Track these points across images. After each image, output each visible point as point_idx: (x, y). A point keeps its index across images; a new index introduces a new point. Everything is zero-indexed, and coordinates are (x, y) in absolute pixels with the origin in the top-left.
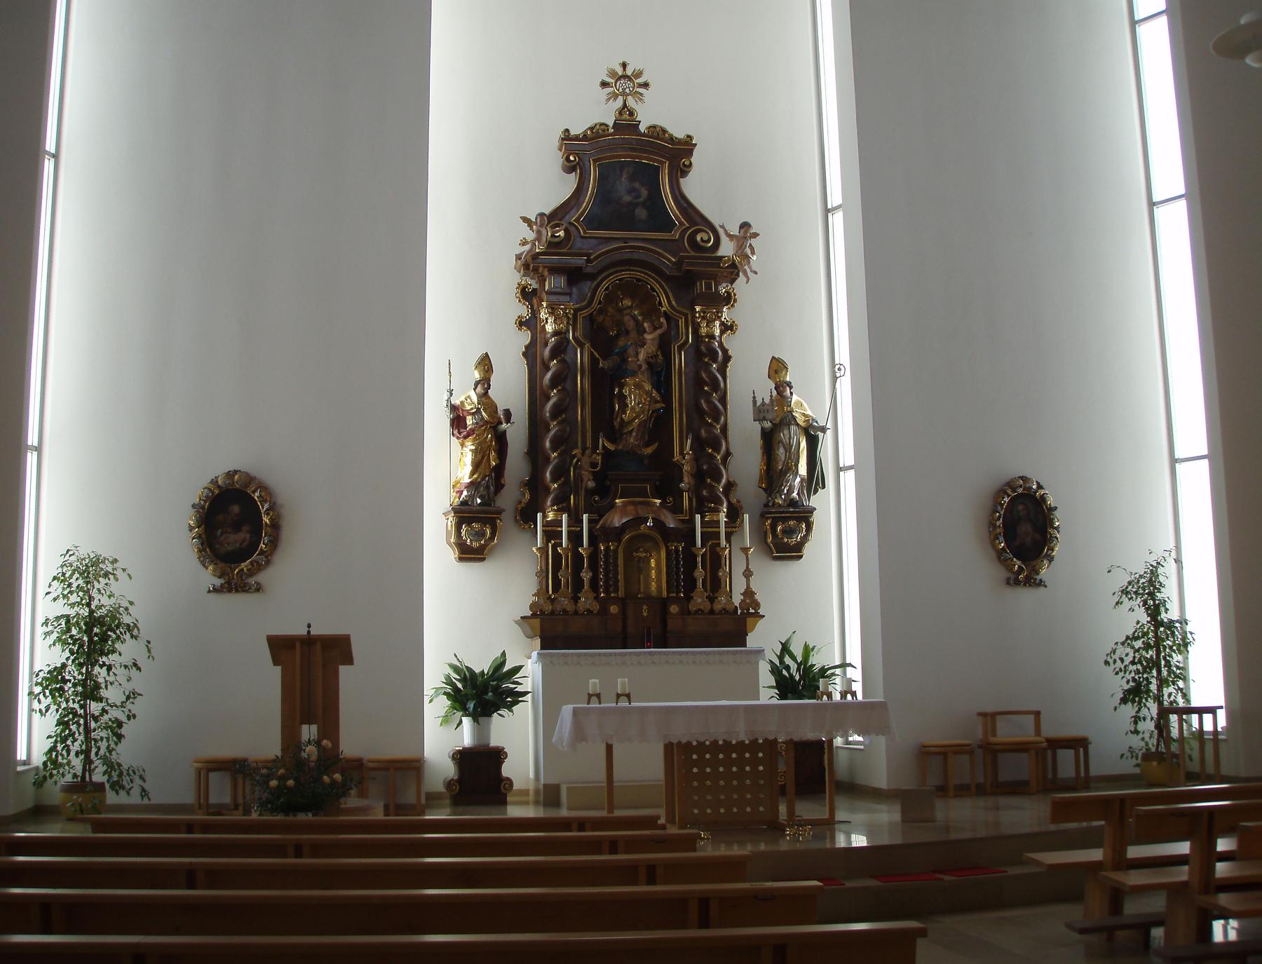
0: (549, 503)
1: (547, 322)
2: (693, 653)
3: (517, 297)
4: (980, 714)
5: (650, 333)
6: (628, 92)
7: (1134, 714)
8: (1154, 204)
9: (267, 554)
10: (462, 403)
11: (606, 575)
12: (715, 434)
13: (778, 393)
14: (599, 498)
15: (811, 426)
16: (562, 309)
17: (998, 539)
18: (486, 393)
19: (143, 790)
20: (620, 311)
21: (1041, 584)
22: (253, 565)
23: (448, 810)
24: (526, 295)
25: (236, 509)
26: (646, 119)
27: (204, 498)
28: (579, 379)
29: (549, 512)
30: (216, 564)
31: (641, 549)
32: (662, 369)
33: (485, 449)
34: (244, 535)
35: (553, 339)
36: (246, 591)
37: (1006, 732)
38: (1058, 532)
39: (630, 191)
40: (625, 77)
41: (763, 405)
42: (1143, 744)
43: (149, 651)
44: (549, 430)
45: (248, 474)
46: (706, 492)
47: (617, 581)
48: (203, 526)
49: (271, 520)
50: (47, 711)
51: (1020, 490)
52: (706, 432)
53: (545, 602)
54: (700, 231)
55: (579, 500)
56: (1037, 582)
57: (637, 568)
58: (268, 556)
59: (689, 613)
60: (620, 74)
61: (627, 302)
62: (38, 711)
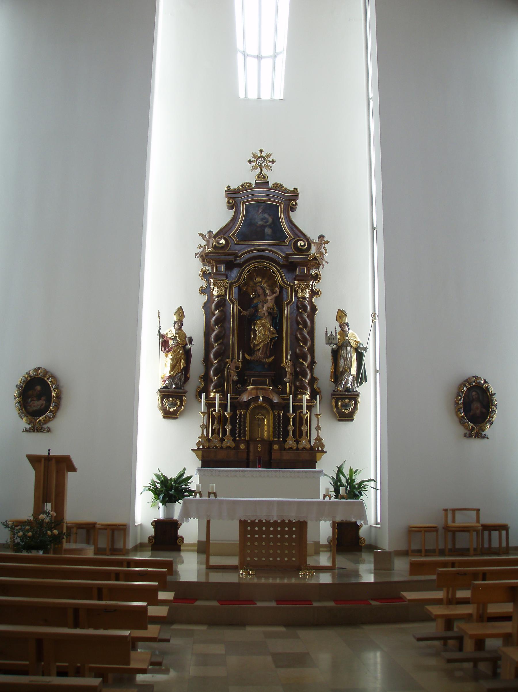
0: (211, 388)
1: (214, 290)
3: (200, 277)
5: (270, 296)
6: (263, 165)
9: (53, 412)
10: (167, 333)
11: (239, 428)
12: (304, 351)
13: (341, 329)
16: (221, 283)
20: (255, 283)
21: (485, 437)
23: (150, 553)
25: (38, 388)
28: (231, 320)
29: (211, 393)
30: (27, 417)
31: (260, 414)
32: (277, 316)
33: (178, 358)
34: (42, 402)
35: (217, 299)
36: (42, 432)
37: (461, 520)
40: (262, 157)
41: (331, 336)
44: (213, 348)
45: (45, 370)
46: (299, 383)
47: (245, 431)
48: (21, 397)
51: (474, 384)
52: (299, 350)
53: (205, 442)
55: (229, 387)
57: (257, 424)
58: (54, 413)
59: (285, 449)
61: (259, 279)
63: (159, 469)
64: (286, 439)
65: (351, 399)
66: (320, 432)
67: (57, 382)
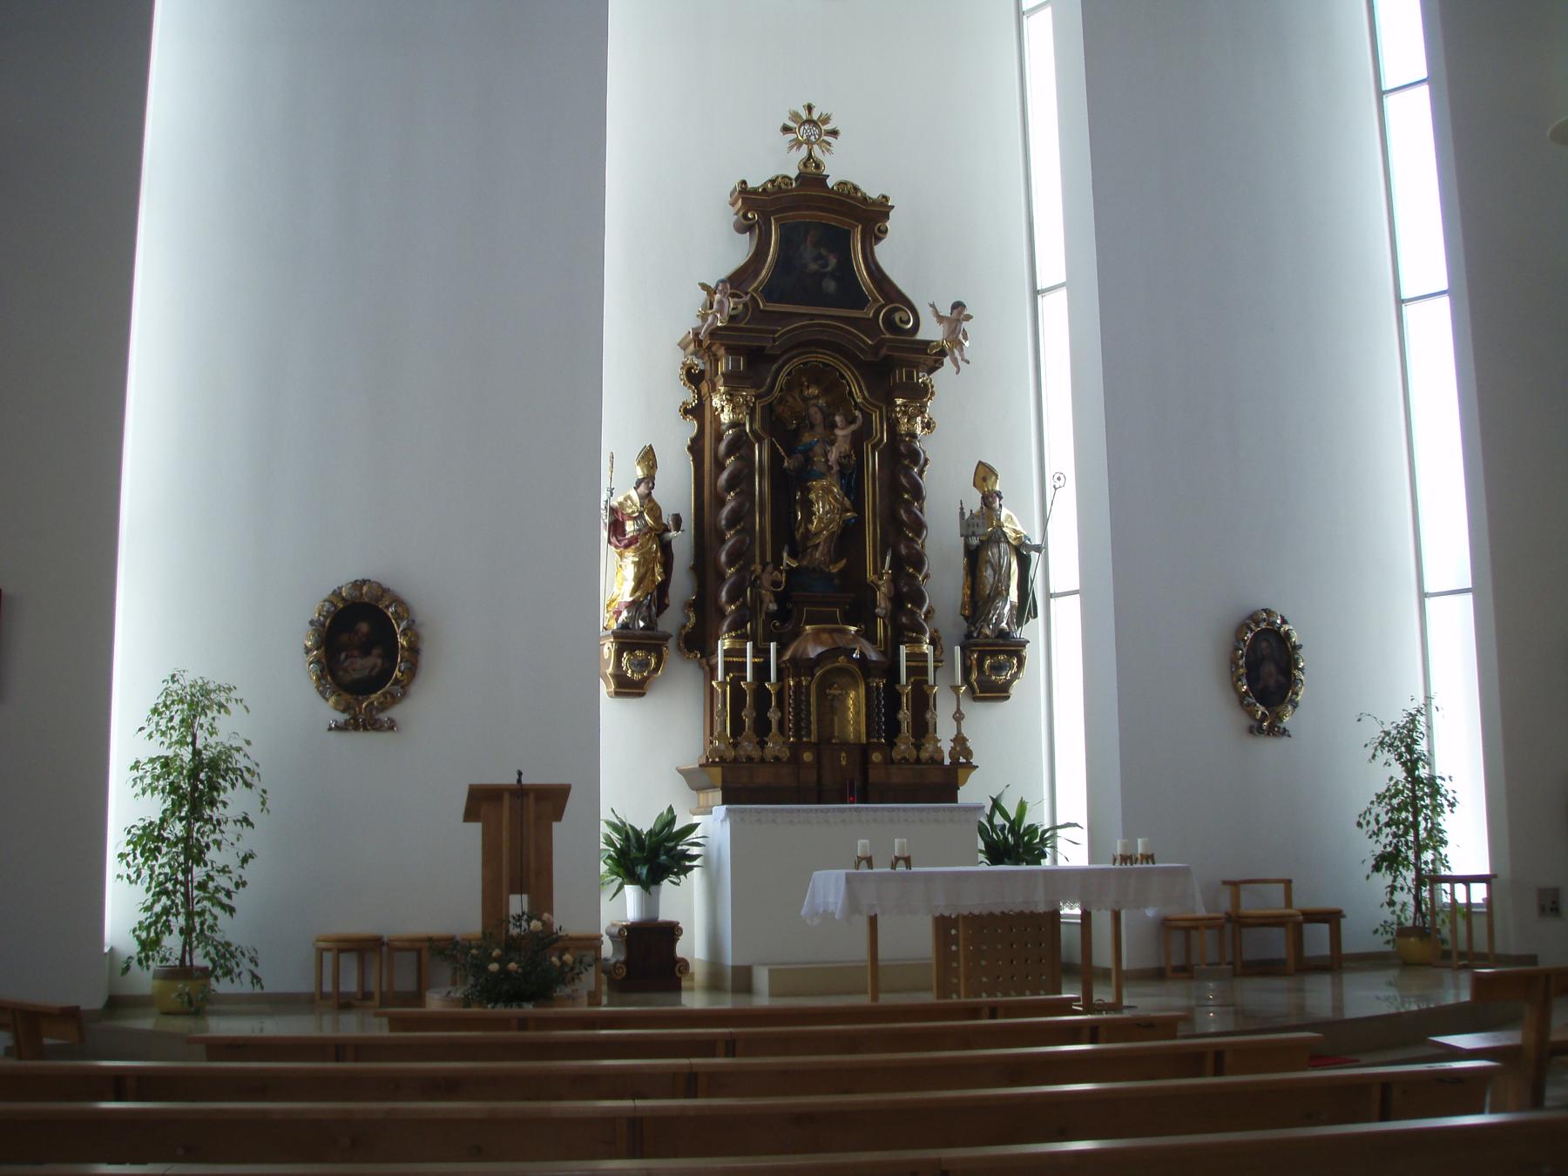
1: (723, 410)
2: (905, 810)
4: (1225, 883)
5: (842, 429)
6: (814, 140)
7: (1390, 883)
8: (1403, 301)
12: (916, 549)
14: (783, 626)
15: (1023, 544)
17: (1240, 680)
18: (649, 494)
19: (254, 976)
20: (805, 400)
21: (1284, 733)
22: (386, 697)
24: (693, 378)
25: (364, 627)
26: (837, 170)
27: (325, 613)
32: (853, 472)
34: (373, 661)
35: (730, 432)
37: (1252, 903)
38: (1303, 673)
39: (815, 260)
40: (810, 121)
41: (973, 519)
42: (1395, 917)
43: (263, 803)
45: (379, 585)
47: (810, 722)
49: (409, 642)
50: (138, 876)
51: (1263, 625)
54: (897, 309)
56: (1281, 730)
57: (831, 707)
58: (404, 686)
59: (892, 762)
60: (805, 118)
62: (125, 876)
63: (613, 811)
64: (895, 740)
65: (1011, 654)
66: (963, 723)
67: (409, 615)
